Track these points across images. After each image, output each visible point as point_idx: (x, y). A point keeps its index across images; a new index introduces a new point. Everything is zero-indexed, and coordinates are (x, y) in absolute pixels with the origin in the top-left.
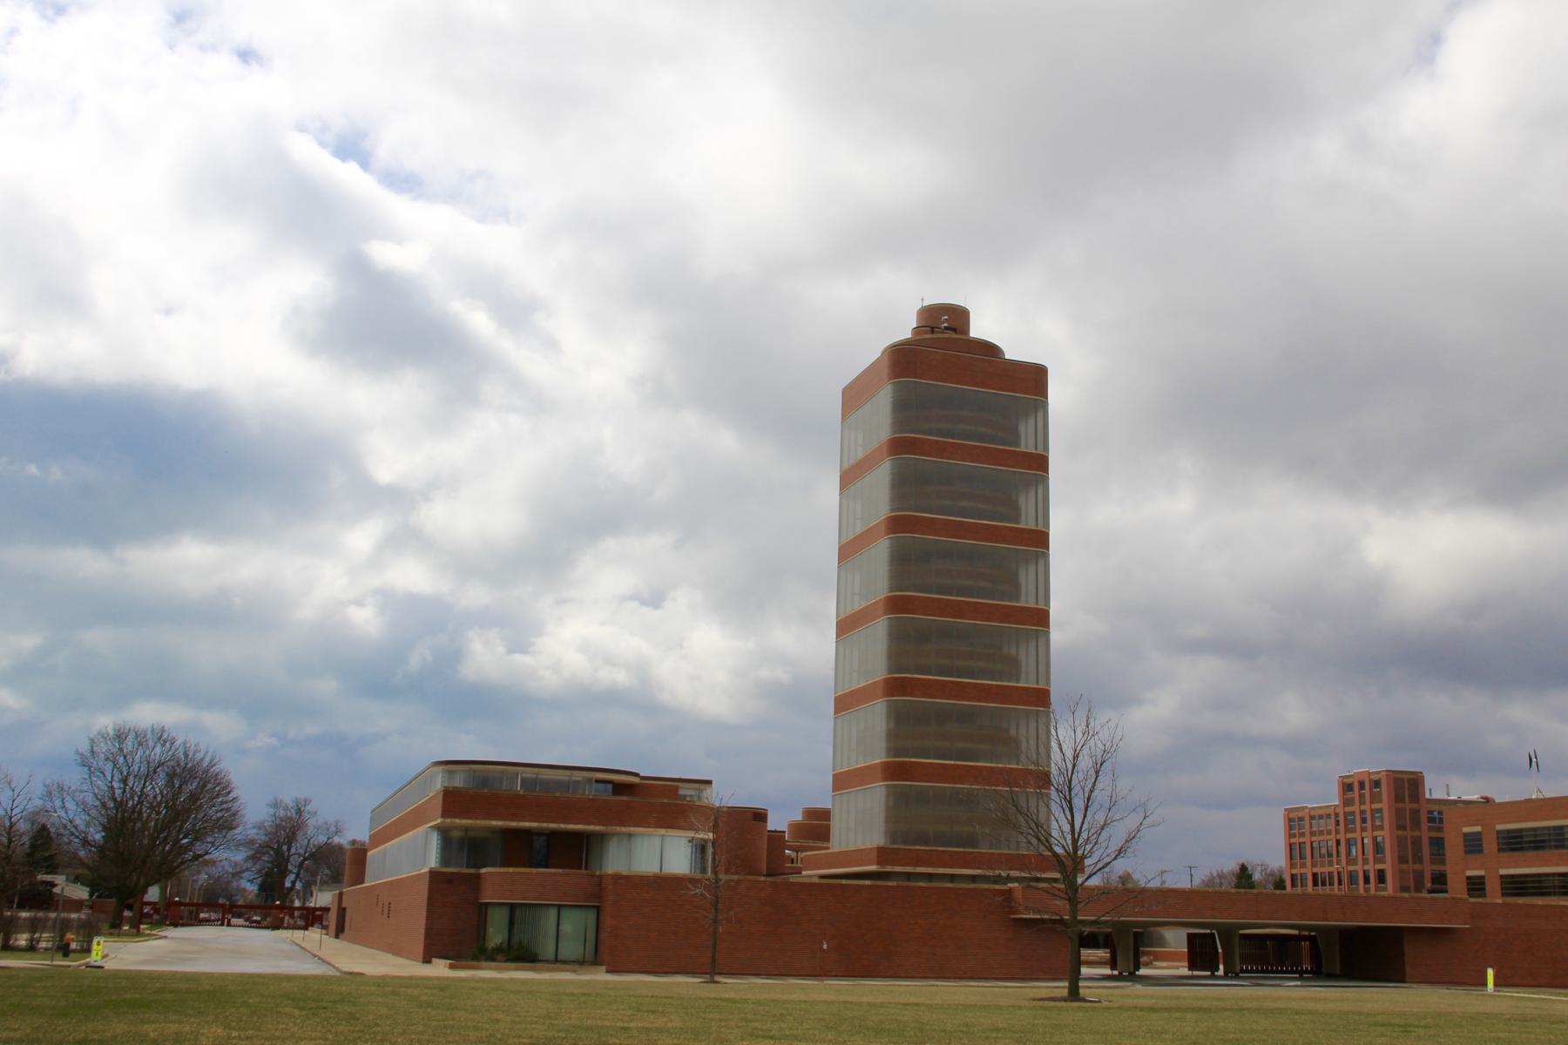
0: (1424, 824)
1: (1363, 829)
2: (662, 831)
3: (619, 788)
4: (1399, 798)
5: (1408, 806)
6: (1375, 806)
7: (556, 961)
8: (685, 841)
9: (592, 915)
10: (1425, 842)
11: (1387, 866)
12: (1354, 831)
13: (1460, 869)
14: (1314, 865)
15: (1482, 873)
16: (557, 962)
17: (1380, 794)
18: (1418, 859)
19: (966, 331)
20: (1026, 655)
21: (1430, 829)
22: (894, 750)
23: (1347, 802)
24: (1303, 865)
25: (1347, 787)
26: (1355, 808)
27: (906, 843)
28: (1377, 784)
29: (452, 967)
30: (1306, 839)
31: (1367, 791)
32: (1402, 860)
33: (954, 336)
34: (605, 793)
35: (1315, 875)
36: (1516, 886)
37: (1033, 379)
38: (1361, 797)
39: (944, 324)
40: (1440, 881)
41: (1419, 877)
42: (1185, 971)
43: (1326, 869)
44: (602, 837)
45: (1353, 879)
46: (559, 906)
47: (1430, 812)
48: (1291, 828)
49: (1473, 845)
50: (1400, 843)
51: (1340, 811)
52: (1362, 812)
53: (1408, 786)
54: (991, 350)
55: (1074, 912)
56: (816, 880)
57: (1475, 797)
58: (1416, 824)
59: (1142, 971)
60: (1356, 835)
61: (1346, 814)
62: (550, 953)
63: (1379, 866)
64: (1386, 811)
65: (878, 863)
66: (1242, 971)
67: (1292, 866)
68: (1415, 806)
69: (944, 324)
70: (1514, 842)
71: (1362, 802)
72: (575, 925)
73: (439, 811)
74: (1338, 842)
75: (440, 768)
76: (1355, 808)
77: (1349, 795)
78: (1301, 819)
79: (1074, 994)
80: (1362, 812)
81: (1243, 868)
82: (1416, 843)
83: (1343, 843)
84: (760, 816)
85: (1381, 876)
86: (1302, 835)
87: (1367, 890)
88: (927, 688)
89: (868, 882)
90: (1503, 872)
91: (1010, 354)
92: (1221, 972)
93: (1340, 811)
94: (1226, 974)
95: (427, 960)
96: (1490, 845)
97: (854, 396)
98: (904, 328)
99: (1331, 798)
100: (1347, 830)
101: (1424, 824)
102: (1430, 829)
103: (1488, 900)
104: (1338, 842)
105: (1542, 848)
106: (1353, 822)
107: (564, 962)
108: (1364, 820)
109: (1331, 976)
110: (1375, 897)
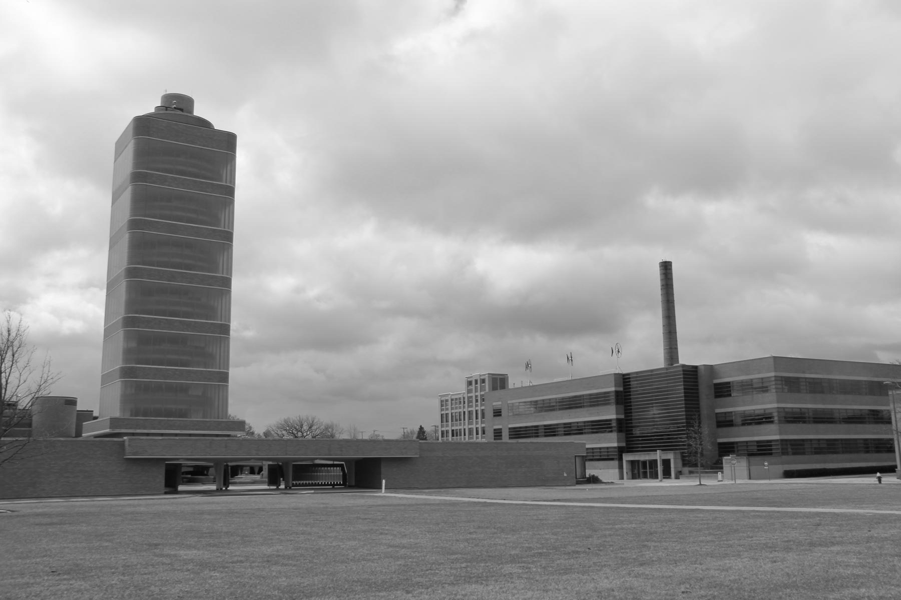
1: (476, 406)
14: (452, 425)
19: (191, 111)
23: (469, 391)
24: (447, 426)
26: (473, 394)
28: (483, 381)
30: (449, 412)
31: (479, 385)
33: (181, 113)
35: (453, 431)
37: (229, 141)
38: (476, 388)
39: (177, 107)
42: (266, 487)
43: (458, 428)
48: (442, 406)
51: (466, 396)
54: (204, 124)
56: (92, 439)
59: (230, 488)
66: (293, 485)
67: (442, 426)
69: (177, 107)
76: (473, 394)
77: (470, 387)
78: (447, 401)
80: (476, 396)
81: (421, 428)
83: (479, 412)
84: (72, 402)
87: (477, 438)
88: (148, 323)
89: (160, 438)
90: (510, 426)
92: (282, 486)
93: (466, 396)
94: (286, 487)
97: (120, 146)
98: (149, 106)
99: (461, 389)
103: (503, 441)
106: (471, 402)
108: (477, 401)
109: (351, 487)
110: (443, 443)
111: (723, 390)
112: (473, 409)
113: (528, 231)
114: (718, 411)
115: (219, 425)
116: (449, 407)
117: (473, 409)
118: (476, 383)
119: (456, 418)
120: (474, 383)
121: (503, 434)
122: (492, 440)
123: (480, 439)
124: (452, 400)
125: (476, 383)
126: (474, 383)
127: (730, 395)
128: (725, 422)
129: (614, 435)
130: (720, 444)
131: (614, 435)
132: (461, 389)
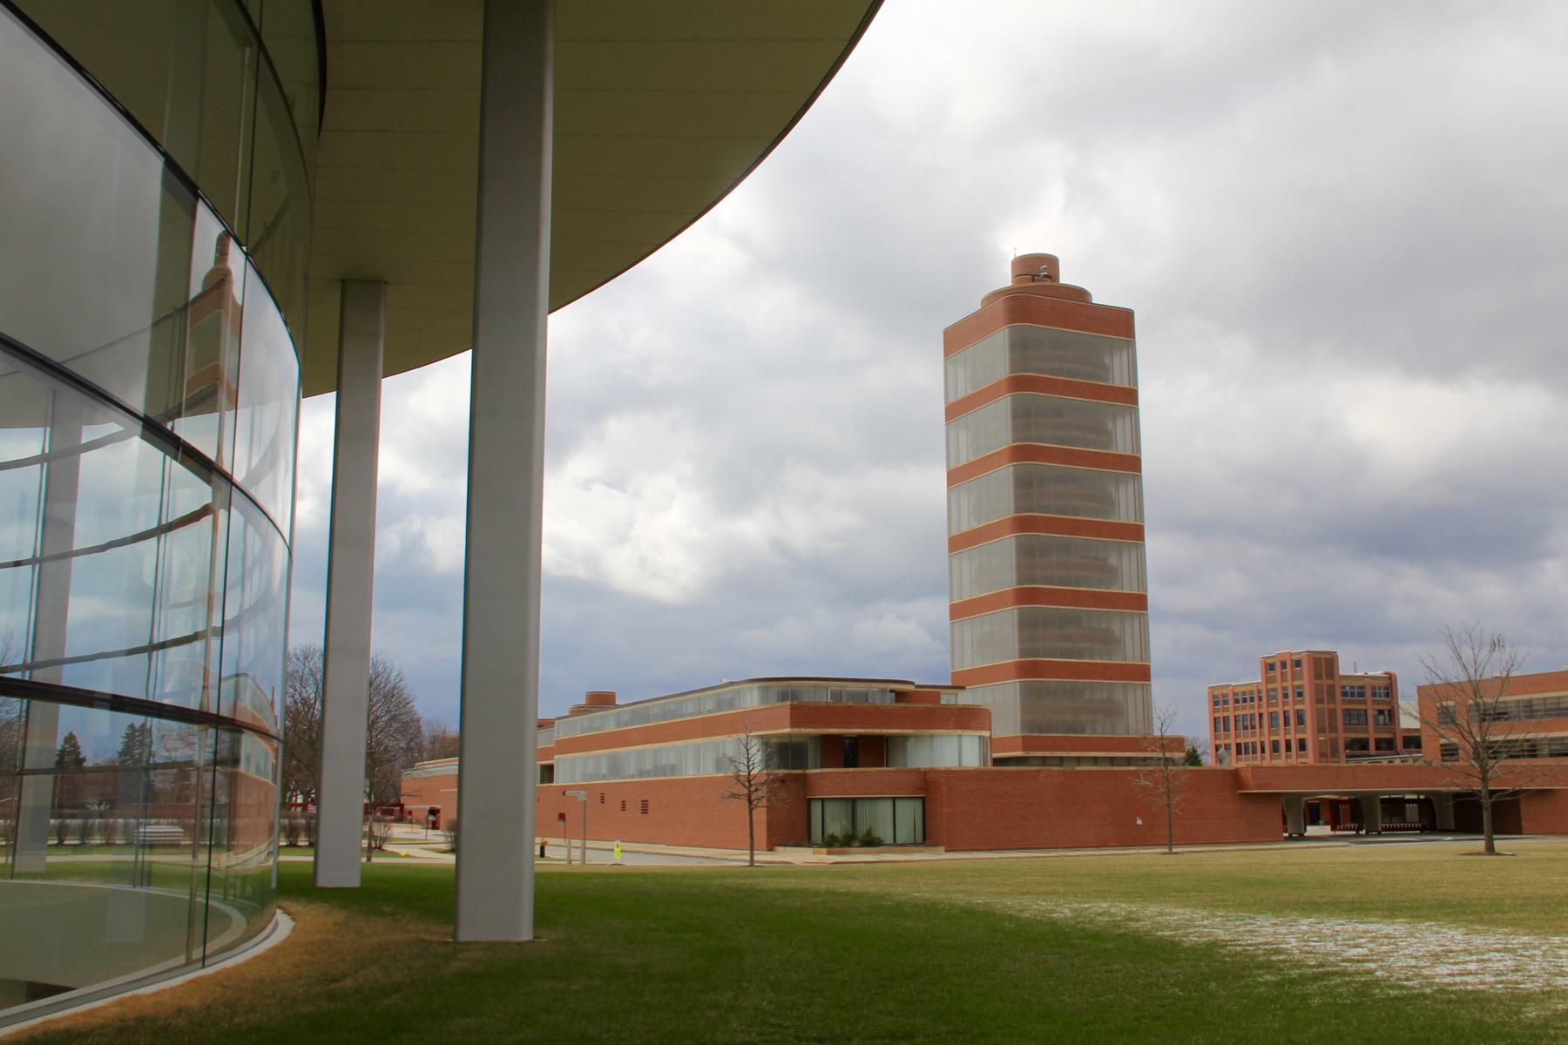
0: (1339, 698)
2: (959, 732)
3: (900, 696)
4: (1318, 676)
5: (1326, 682)
7: (895, 843)
8: (976, 741)
9: (918, 805)
11: (1308, 735)
12: (1276, 705)
14: (1237, 736)
16: (896, 844)
17: (1301, 672)
18: (1333, 729)
20: (1126, 565)
21: (1343, 702)
23: (1268, 680)
26: (1278, 685)
27: (1040, 731)
28: (1298, 663)
29: (829, 853)
30: (1230, 714)
31: (1288, 670)
32: (1321, 730)
34: (889, 700)
35: (1238, 745)
41: (1334, 743)
43: (1250, 740)
44: (905, 737)
45: (1275, 747)
46: (894, 799)
48: (1216, 703)
50: (1319, 715)
52: (1284, 688)
53: (1325, 664)
54: (1080, 294)
57: (1379, 673)
58: (1332, 698)
61: (1268, 691)
62: (890, 841)
63: (1274, 738)
65: (1024, 749)
68: (1330, 682)
71: (1283, 678)
72: (909, 812)
74: (1261, 715)
75: (757, 685)
76: (1278, 685)
77: (1271, 673)
79: (1490, 850)
80: (1284, 688)
82: (1332, 713)
88: (1055, 597)
91: (1096, 300)
95: (770, 849)
97: (957, 339)
98: (1004, 278)
100: (1269, 705)
101: (1339, 698)
102: (1343, 702)
104: (1261, 715)
107: (902, 845)
112: (1279, 709)
113: (1436, 356)
117: (1279, 709)
119: (1247, 724)
122: (1436, 763)
123: (1294, 759)
129: (440, 838)
131: (440, 838)
132: (1254, 678)
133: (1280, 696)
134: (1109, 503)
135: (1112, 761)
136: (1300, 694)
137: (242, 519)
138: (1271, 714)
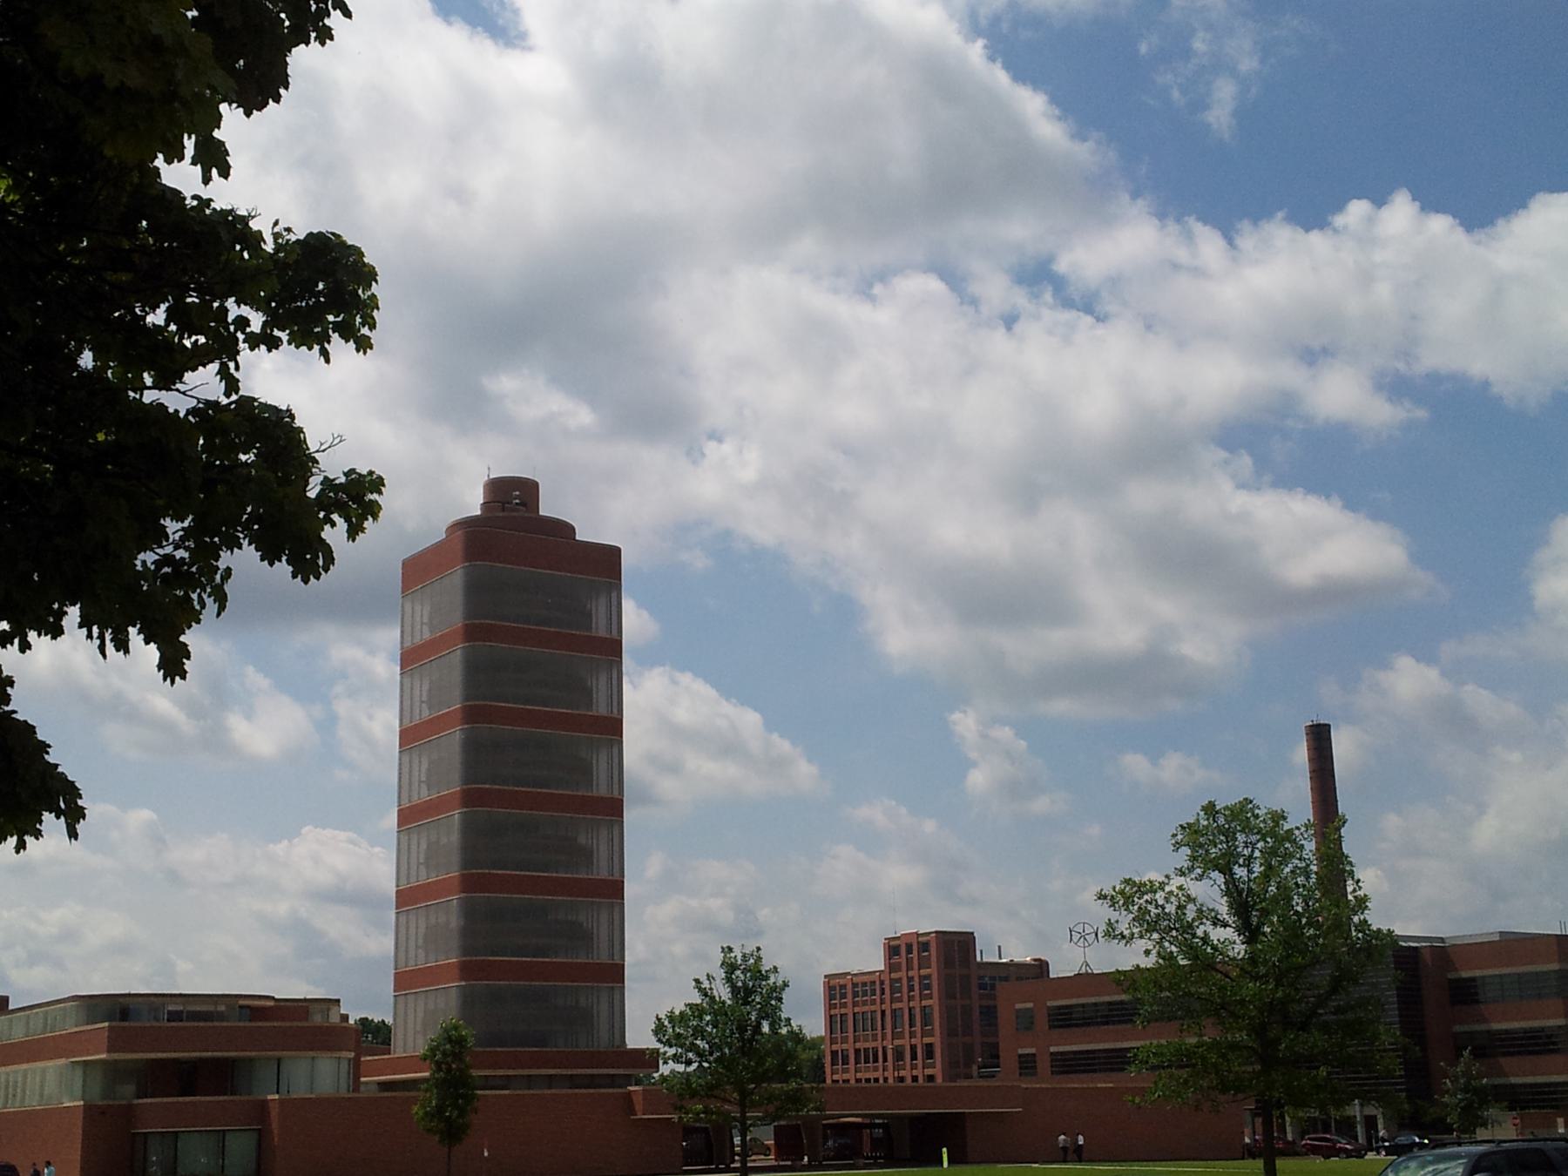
2: (311, 1054)
6: (923, 972)
10: (976, 1014)
11: (936, 1040)
12: (900, 1000)
13: (1014, 1047)
15: (1033, 1051)
22: (466, 950)
23: (892, 967)
24: (844, 1040)
25: (893, 949)
28: (925, 947)
30: (849, 1011)
35: (857, 1051)
36: (1067, 1064)
40: (993, 1057)
44: (251, 1060)
47: (981, 978)
49: (1026, 1022)
52: (910, 979)
55: (743, 1113)
60: (903, 1005)
63: (927, 1040)
64: (935, 977)
67: (833, 1041)
70: (1064, 1019)
73: (105, 1046)
74: (883, 1012)
76: (902, 974)
78: (843, 987)
80: (910, 979)
83: (888, 1013)
85: (929, 1051)
86: (844, 1005)
96: (1044, 1065)
98: (473, 503)
104: (883, 1012)
105: (1089, 1025)
111: (1465, 994)
114: (1458, 1028)
115: (596, 1059)
116: (849, 999)
118: (909, 951)
120: (903, 950)
121: (1039, 1065)
124: (855, 985)
125: (909, 951)
126: (903, 950)
127: (1477, 1002)
128: (1489, 1047)
130: (1020, 1056)
132: (875, 962)
133: (905, 990)
134: (586, 771)
135: (530, 1081)
136: (928, 987)
137: (1303, 571)
138: (894, 1011)
